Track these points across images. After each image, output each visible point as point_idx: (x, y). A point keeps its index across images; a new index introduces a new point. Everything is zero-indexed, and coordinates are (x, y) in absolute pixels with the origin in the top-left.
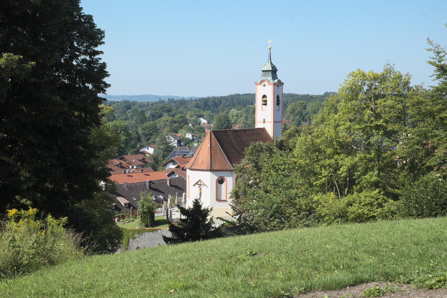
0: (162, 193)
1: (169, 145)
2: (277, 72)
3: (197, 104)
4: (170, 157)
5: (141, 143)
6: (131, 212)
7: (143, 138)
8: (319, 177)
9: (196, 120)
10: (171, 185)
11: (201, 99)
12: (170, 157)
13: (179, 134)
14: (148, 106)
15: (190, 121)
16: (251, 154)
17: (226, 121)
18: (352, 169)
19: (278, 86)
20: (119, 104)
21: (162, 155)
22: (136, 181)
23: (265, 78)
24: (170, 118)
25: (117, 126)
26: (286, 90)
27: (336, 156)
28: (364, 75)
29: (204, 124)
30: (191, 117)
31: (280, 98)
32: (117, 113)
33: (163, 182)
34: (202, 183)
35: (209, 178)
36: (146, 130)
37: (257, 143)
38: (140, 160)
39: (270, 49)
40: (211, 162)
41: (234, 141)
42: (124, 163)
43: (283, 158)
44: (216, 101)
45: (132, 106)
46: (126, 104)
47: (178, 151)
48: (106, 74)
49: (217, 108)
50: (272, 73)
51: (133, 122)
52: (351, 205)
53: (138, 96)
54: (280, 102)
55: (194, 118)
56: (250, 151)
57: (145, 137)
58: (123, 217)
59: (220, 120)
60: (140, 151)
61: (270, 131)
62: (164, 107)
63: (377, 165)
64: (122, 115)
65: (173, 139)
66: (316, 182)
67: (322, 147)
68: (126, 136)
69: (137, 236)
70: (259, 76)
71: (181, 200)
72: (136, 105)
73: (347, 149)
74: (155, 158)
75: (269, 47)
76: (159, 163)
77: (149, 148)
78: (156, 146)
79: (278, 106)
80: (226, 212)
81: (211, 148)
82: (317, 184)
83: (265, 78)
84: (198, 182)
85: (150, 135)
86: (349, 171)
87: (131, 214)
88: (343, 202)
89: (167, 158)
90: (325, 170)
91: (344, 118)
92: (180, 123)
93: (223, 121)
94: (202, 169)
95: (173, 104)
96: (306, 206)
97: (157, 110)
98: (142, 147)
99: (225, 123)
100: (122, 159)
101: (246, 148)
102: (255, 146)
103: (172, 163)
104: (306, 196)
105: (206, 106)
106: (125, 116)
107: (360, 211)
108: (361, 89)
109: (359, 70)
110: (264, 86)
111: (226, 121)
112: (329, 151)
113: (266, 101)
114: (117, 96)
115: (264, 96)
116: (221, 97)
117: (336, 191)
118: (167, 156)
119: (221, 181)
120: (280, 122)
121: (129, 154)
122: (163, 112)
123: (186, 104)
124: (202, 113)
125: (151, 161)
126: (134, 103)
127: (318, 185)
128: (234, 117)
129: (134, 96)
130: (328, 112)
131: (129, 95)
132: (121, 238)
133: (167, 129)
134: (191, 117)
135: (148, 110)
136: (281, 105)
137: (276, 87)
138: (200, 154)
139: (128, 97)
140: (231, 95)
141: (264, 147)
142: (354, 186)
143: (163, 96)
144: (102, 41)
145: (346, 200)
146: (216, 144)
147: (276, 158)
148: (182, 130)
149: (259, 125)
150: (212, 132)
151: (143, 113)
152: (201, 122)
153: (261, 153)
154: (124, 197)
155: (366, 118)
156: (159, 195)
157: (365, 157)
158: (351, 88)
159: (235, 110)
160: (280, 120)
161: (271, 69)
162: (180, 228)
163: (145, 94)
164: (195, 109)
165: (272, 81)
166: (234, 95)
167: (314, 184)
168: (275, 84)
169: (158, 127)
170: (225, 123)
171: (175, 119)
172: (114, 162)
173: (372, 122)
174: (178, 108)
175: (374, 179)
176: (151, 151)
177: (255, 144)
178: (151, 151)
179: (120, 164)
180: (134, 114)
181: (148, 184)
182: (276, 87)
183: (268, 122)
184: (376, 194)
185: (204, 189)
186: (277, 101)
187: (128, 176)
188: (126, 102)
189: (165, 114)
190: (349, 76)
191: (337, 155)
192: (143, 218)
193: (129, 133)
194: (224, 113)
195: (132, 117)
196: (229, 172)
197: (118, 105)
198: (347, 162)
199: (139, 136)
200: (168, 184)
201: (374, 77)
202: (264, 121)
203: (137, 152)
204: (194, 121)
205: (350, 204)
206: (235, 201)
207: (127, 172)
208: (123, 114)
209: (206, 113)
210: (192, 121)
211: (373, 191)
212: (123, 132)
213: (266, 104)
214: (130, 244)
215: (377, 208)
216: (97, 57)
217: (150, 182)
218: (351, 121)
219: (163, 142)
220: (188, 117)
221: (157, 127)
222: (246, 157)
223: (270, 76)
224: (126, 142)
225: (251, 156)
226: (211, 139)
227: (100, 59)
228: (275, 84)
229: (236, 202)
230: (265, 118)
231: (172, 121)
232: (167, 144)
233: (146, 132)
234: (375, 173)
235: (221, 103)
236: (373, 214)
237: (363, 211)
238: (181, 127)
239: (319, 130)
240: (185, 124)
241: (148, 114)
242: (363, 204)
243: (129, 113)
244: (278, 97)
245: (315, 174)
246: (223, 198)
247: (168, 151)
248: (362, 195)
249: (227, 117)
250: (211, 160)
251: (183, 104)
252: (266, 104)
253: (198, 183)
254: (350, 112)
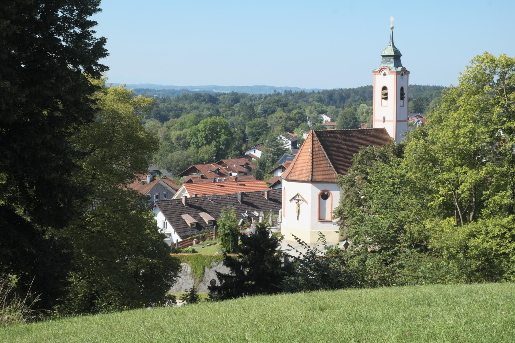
0: (258, 209)
1: (280, 147)
2: (401, 58)
3: (320, 97)
4: (279, 163)
5: (247, 144)
6: (214, 232)
7: (250, 139)
8: (435, 196)
9: (317, 117)
10: (270, 199)
11: (325, 92)
12: (279, 163)
13: (295, 134)
14: (260, 98)
15: (309, 118)
16: (361, 162)
17: (353, 119)
18: (479, 187)
19: (402, 75)
20: (226, 96)
21: (271, 160)
22: (228, 193)
23: (386, 65)
24: (284, 113)
25: (216, 123)
26: (413, 80)
27: (458, 169)
28: (493, 60)
29: (326, 122)
30: (311, 113)
31: (405, 91)
32: (221, 107)
33: (259, 194)
34: (300, 198)
35: (310, 192)
36: (254, 128)
37: (368, 149)
38: (243, 166)
39: (392, 29)
40: (312, 172)
41: (344, 143)
42: (223, 169)
43: (392, 168)
44: (344, 94)
45: (241, 99)
46: (234, 97)
47: (290, 155)
48: (103, 54)
49: (344, 103)
50: (394, 59)
51: (240, 118)
52: (474, 236)
53: (250, 87)
54: (405, 96)
55: (315, 114)
56: (359, 158)
57: (252, 136)
58: (204, 239)
59: (344, 117)
60: (246, 154)
61: (391, 132)
62: (278, 101)
63: (510, 182)
64: (227, 109)
65: (285, 139)
66: (432, 203)
67: (440, 156)
68: (227, 135)
69: (215, 264)
70: (379, 63)
71: (277, 218)
72: (246, 98)
73: (472, 159)
74: (262, 164)
75: (391, 27)
76: (266, 169)
77: (257, 151)
78: (264, 148)
79: (402, 101)
80: (288, 245)
81: (312, 153)
82: (432, 205)
83: (386, 65)
84: (296, 196)
85: (260, 133)
86: (475, 188)
87: (214, 234)
88: (464, 232)
89: (277, 163)
90: (443, 187)
91: (466, 118)
92: (297, 121)
93: (349, 119)
94: (295, 179)
95: (290, 98)
96: (419, 234)
97: (269, 104)
98: (248, 149)
99: (351, 121)
100: (221, 163)
101: (354, 155)
102: (366, 152)
103: (281, 169)
104: (419, 222)
105: (331, 99)
106: (231, 111)
107: (486, 245)
108: (490, 78)
109: (487, 53)
110: (384, 75)
111: (353, 119)
112: (448, 161)
114: (225, 87)
115: (384, 88)
116: (350, 89)
117: (458, 217)
118: (277, 161)
119: (324, 196)
120: (404, 121)
121: (230, 158)
122: (277, 107)
123: (307, 97)
124: (324, 108)
125: (255, 167)
126: (244, 96)
127: (434, 207)
128: (364, 115)
129: (245, 87)
130: (446, 109)
131: (240, 86)
132: (178, 269)
133: (279, 128)
134: (311, 113)
135: (259, 104)
136: (406, 99)
137: (399, 76)
138: (299, 161)
139: (238, 88)
140: (362, 87)
141: (377, 153)
142: (482, 210)
143: (281, 88)
144: (98, 7)
145: (467, 228)
146: (319, 149)
147: (383, 169)
148: (299, 129)
149: (377, 125)
150: (314, 133)
151: (251, 107)
152: (323, 120)
153: (373, 161)
154: (208, 213)
155: (495, 117)
156: (253, 211)
157: (494, 170)
158: (475, 77)
159: (365, 105)
160: (405, 119)
161: (393, 54)
162: (239, 262)
163: (260, 85)
164: (316, 103)
165: (394, 70)
166: (365, 87)
167: (429, 205)
168: (398, 73)
169: (269, 125)
170: (351, 121)
171: (291, 115)
172: (210, 167)
173: (504, 123)
174: (297, 103)
175: (507, 201)
176: (258, 154)
177: (365, 149)
178: (258, 154)
179: (218, 169)
180: (242, 109)
181: (239, 197)
182: (399, 76)
183: (390, 121)
184: (508, 222)
185: (303, 205)
186: (401, 94)
187: (218, 185)
188: (234, 94)
189: (279, 109)
190: (473, 61)
191: (459, 167)
192: (224, 241)
193: (231, 132)
194: (351, 109)
195: (239, 113)
196: (335, 185)
197: (224, 97)
198: (470, 177)
199: (245, 135)
200: (266, 197)
201: (506, 63)
202: (384, 120)
203: (242, 155)
204: (314, 118)
205: (472, 235)
206: (340, 223)
207: (217, 181)
208: (230, 108)
209: (329, 109)
210: (312, 118)
211: (505, 217)
212: (223, 131)
213: (386, 98)
214: (206, 275)
215: (510, 242)
216: (90, 29)
217: (243, 194)
218: (475, 121)
219: (273, 143)
220: (307, 113)
221: (268, 125)
222: (355, 166)
223: (391, 63)
224: (227, 142)
225: (360, 164)
226: (313, 142)
227: (94, 32)
228: (398, 73)
229: (342, 224)
230: (384, 116)
231: (286, 118)
232: (277, 146)
233: (254, 131)
234: (508, 193)
235: (349, 96)
236: (504, 251)
237: (490, 245)
238: (298, 125)
239: (435, 133)
240: (303, 121)
241: (259, 109)
242: (491, 235)
243: (237, 107)
244: (402, 89)
245: (430, 192)
246: (328, 217)
247: (279, 155)
248: (490, 222)
249: (354, 114)
250: (312, 169)
251: (303, 97)
252: (386, 98)
253: (296, 198)
254: (475, 110)
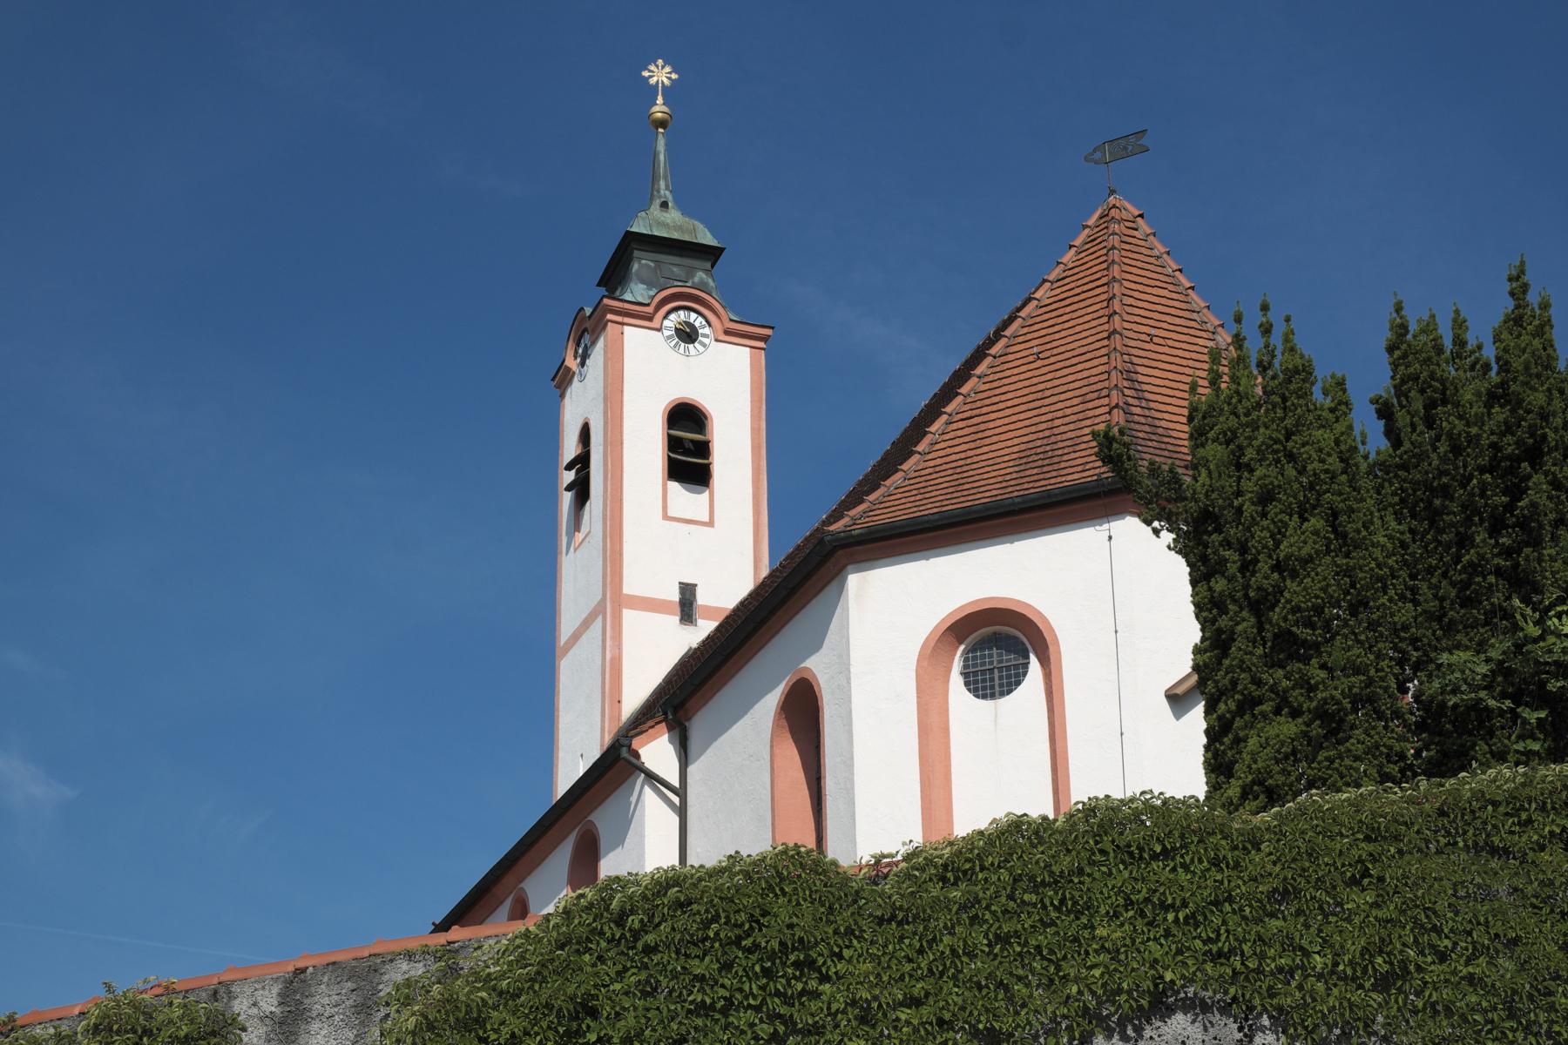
113: (703, 449)
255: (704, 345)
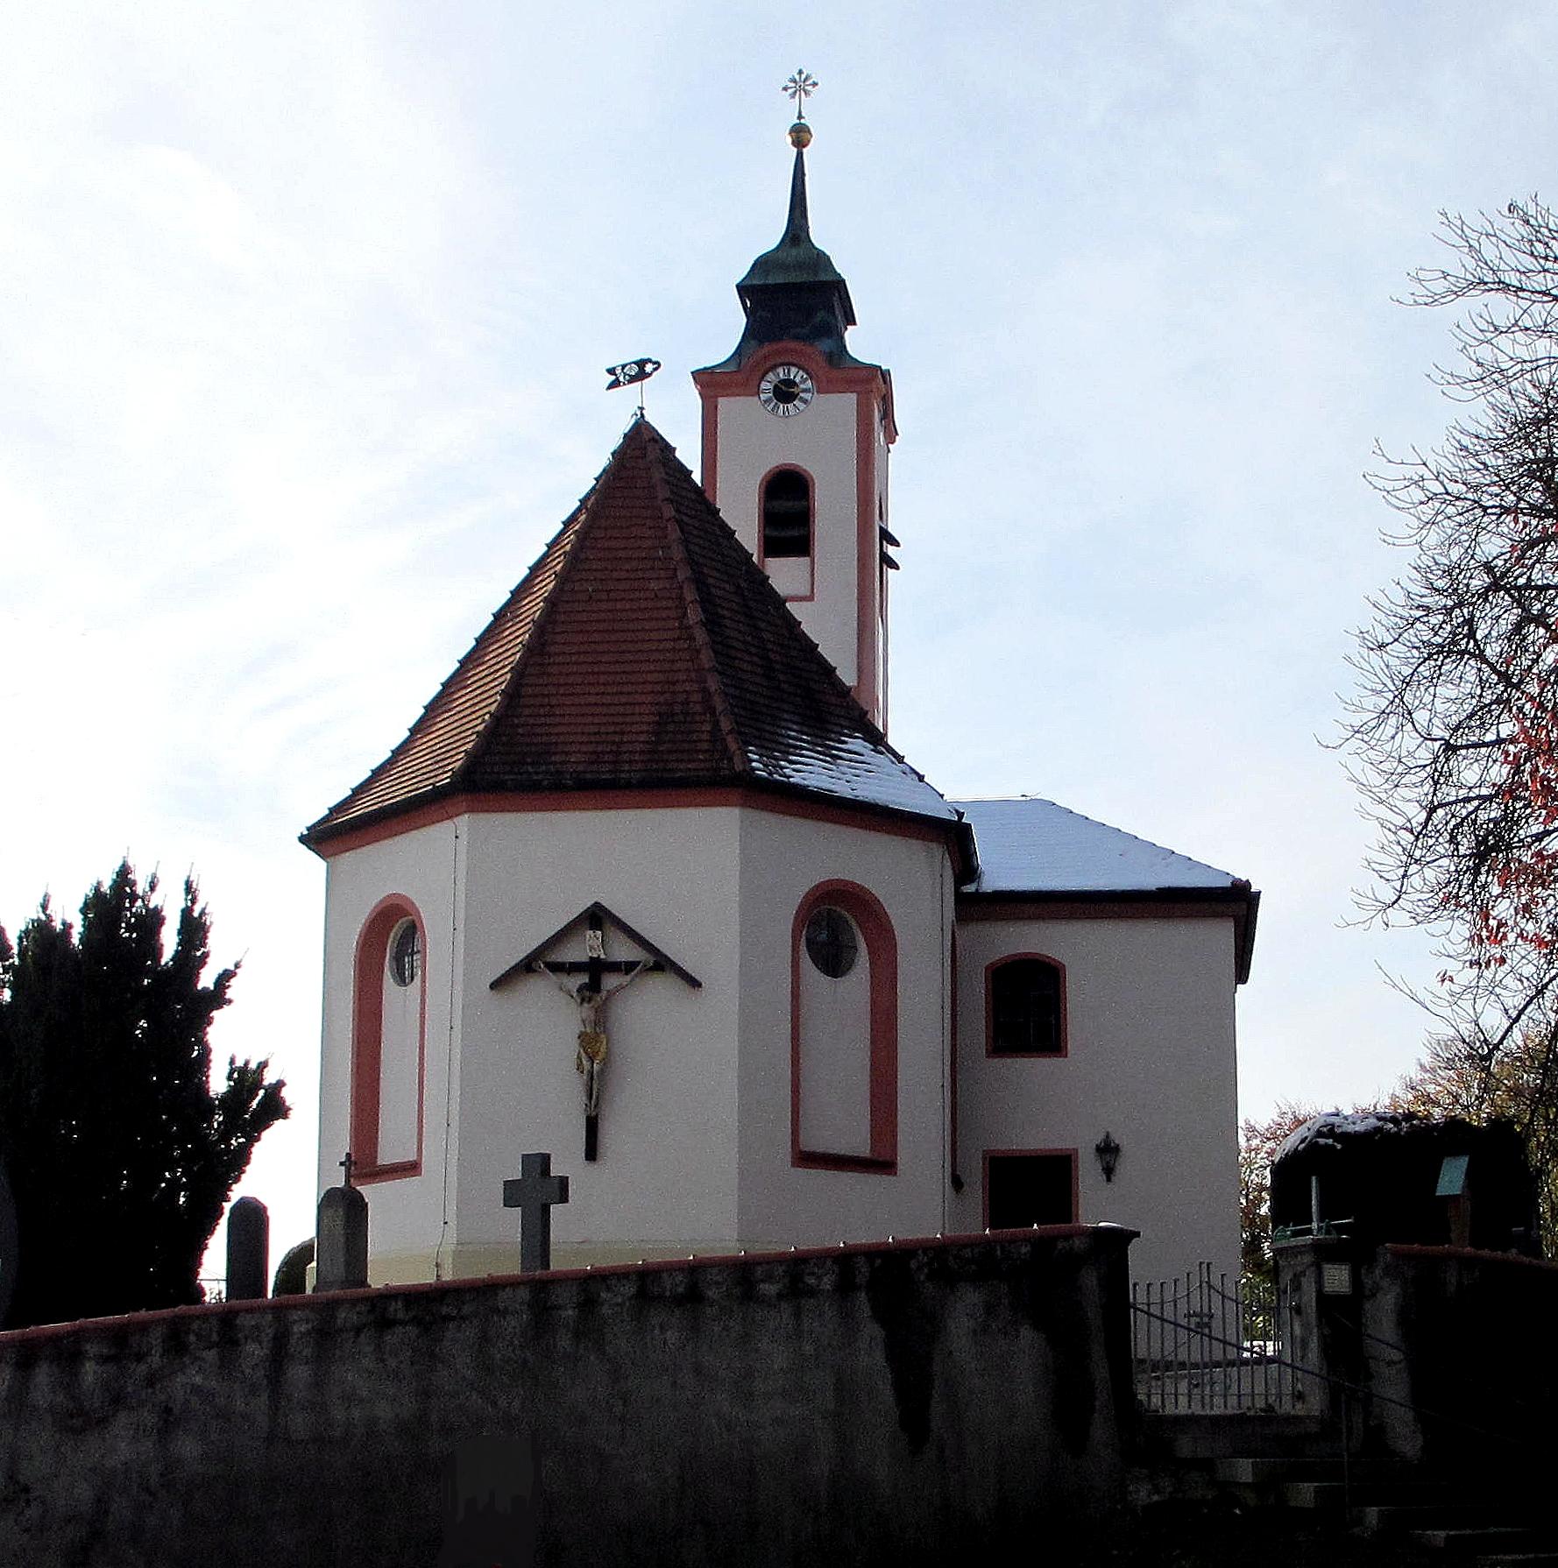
110: (785, 393)
255: (805, 401)
